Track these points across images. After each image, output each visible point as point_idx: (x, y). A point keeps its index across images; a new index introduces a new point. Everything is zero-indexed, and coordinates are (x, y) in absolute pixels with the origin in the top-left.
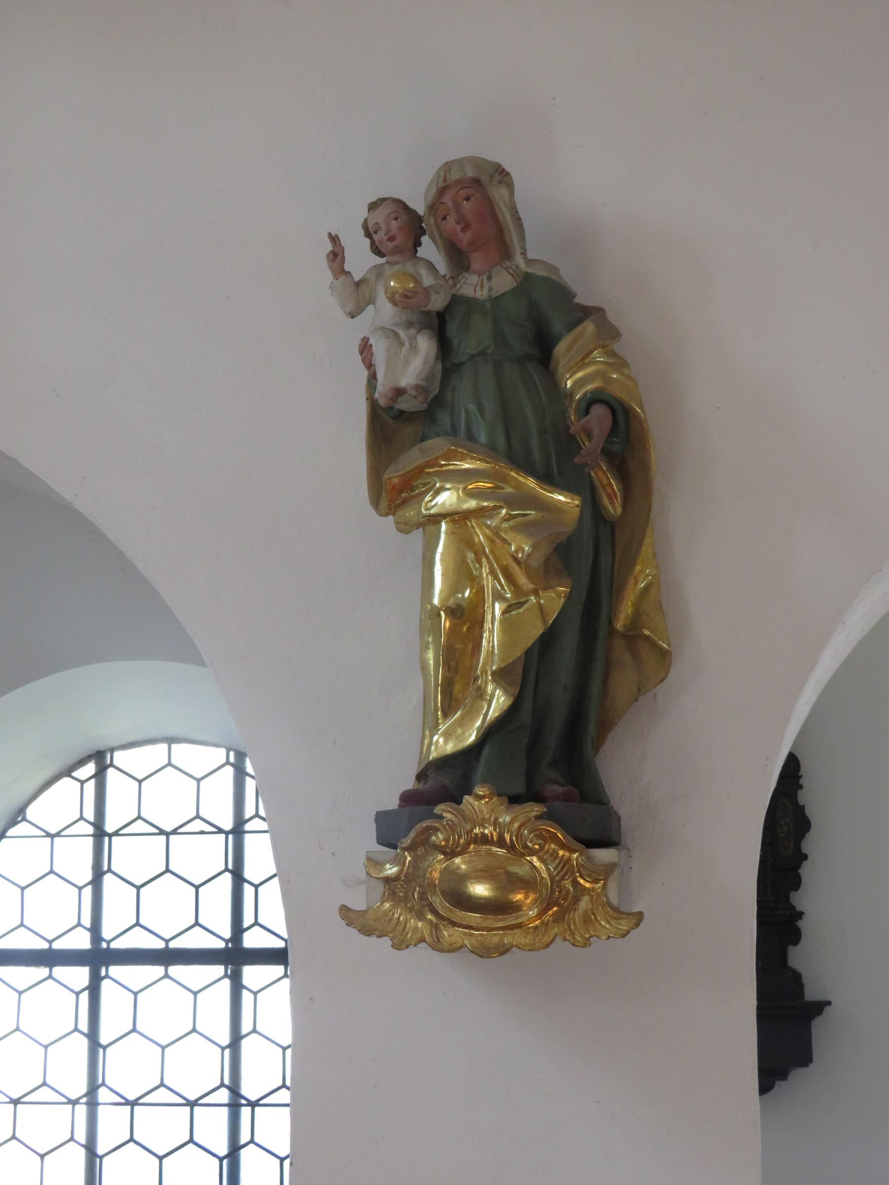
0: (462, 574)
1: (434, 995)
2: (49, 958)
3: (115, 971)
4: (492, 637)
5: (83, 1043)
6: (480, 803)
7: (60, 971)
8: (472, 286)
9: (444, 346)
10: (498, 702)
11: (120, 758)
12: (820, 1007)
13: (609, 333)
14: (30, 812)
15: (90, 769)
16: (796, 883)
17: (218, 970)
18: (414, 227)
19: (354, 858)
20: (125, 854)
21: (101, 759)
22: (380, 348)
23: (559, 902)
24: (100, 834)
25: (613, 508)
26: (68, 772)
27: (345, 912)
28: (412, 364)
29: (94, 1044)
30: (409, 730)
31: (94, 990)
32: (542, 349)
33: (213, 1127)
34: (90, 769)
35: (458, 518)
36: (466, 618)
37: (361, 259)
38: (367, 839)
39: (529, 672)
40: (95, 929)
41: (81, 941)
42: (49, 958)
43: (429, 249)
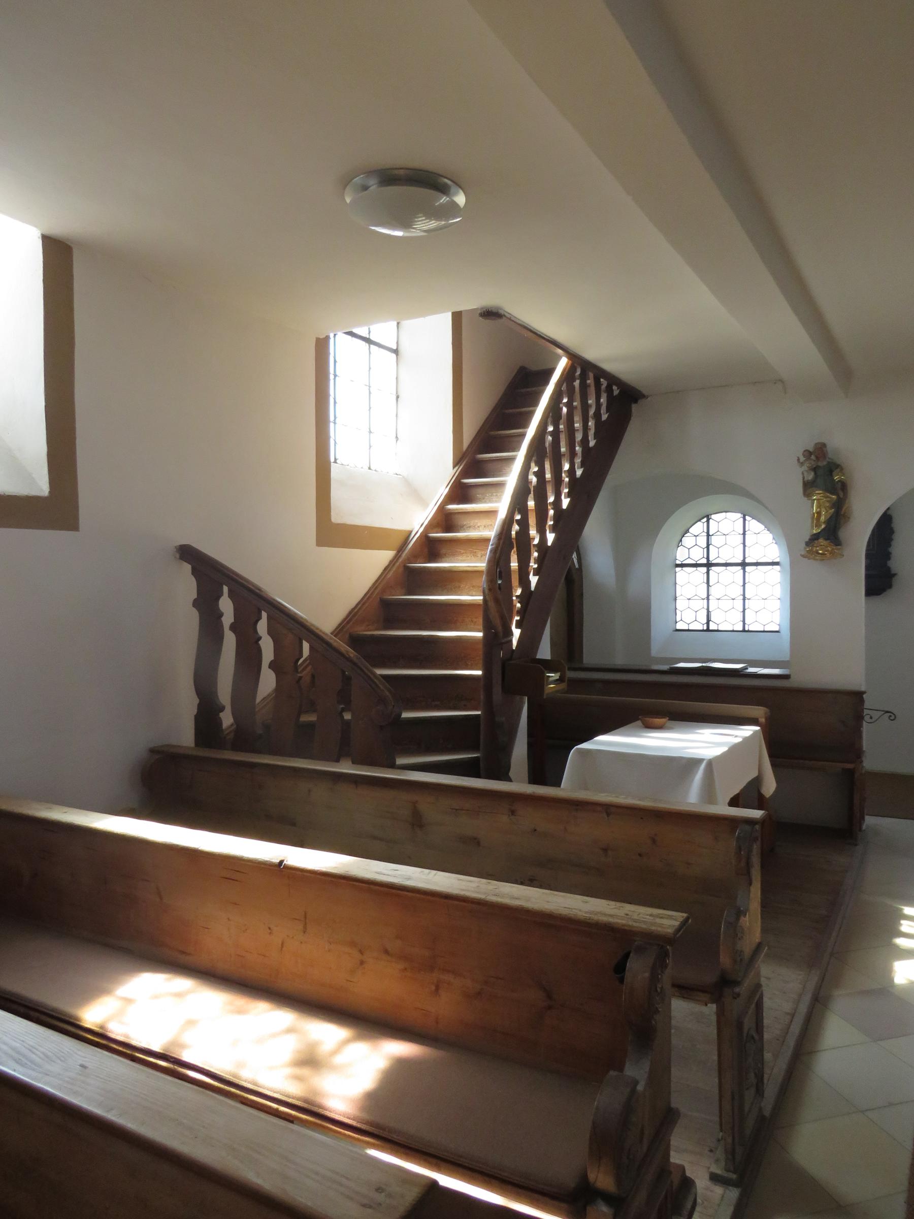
0: (818, 507)
1: (814, 567)
2: (696, 565)
3: (713, 568)
4: (823, 518)
5: (706, 585)
6: (821, 540)
7: (699, 569)
8: (820, 464)
9: (815, 474)
10: (823, 526)
11: (713, 516)
12: (895, 575)
13: (842, 469)
14: (690, 530)
15: (705, 519)
16: (890, 546)
17: (740, 568)
18: (810, 453)
19: (801, 547)
20: (714, 540)
21: (708, 518)
22: (806, 474)
23: (832, 553)
24: (708, 535)
25: (841, 496)
26: (700, 520)
27: (802, 556)
28: (810, 476)
29: (708, 586)
30: (808, 530)
31: (708, 573)
32: (831, 472)
33: (739, 604)
34: (705, 519)
35: (818, 500)
36: (819, 513)
37: (802, 459)
38: (804, 545)
39: (828, 522)
40: (708, 558)
41: (704, 561)
42: (696, 565)
43: (813, 457)
